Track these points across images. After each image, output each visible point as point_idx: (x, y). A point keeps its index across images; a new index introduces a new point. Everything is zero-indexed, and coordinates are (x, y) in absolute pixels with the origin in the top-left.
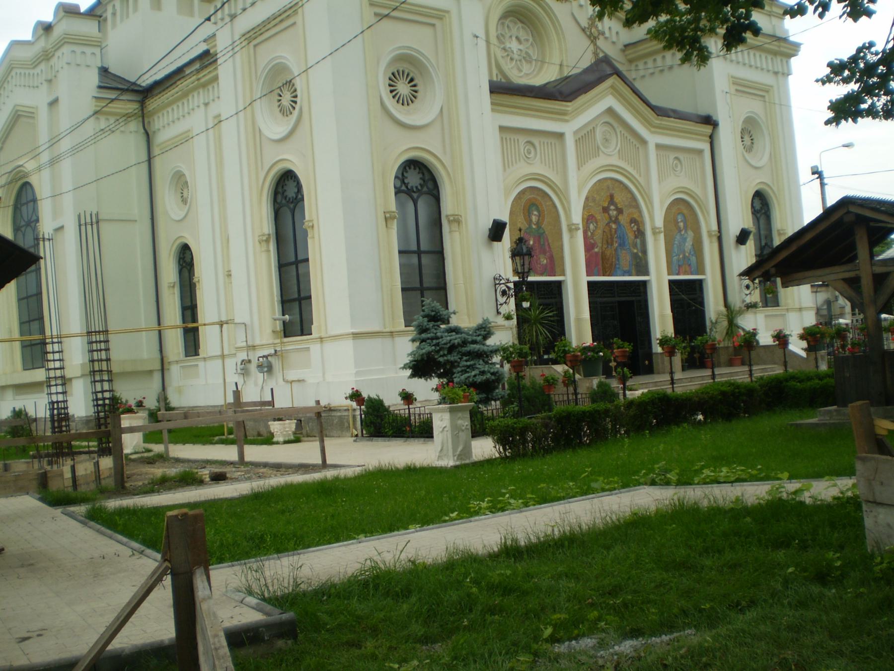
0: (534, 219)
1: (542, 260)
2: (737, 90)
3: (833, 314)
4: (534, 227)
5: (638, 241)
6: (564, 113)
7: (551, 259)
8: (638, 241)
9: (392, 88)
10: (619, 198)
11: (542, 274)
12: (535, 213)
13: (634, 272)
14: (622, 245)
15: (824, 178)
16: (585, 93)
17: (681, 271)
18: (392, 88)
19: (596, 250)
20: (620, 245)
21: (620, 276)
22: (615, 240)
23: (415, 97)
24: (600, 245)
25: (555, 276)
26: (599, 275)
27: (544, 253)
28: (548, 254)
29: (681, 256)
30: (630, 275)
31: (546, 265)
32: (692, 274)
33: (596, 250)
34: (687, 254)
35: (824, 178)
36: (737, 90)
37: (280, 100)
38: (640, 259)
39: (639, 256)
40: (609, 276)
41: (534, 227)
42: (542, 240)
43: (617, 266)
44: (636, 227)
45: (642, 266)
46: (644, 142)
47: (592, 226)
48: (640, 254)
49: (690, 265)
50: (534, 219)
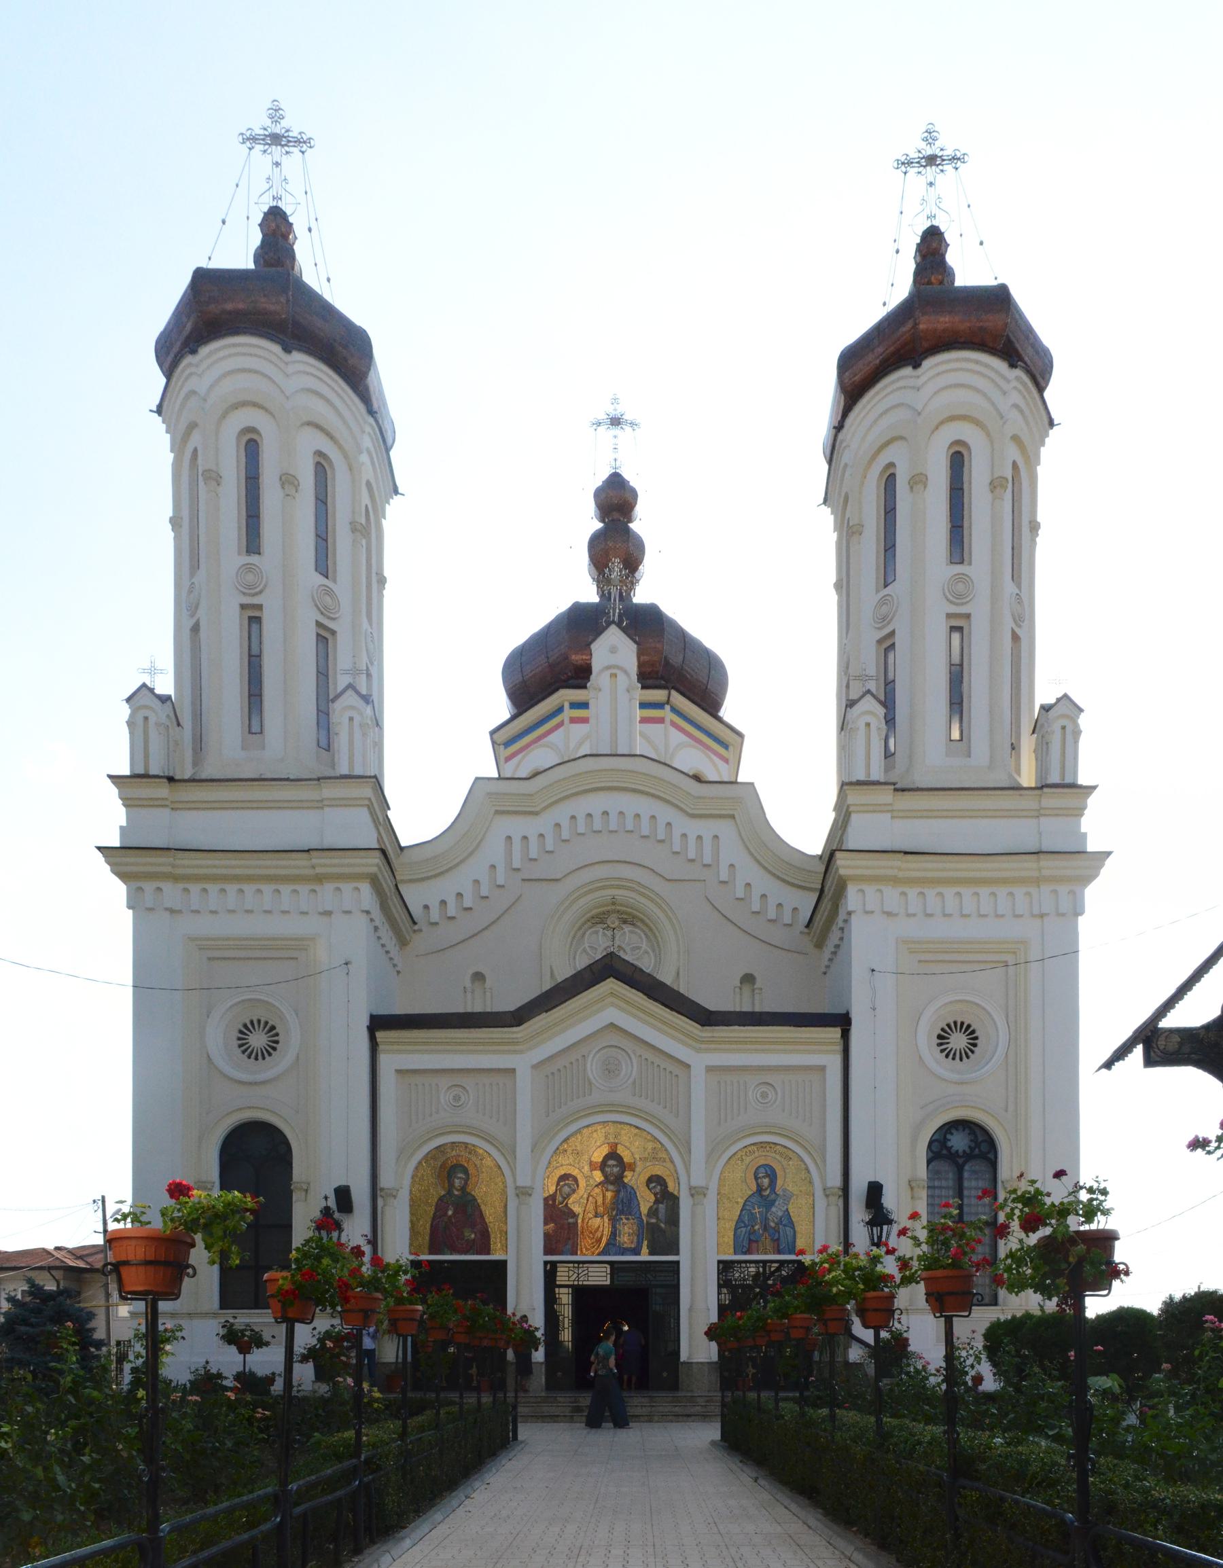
6: (515, 1042)
11: (466, 1253)
44: (659, 1187)
48: (663, 1225)
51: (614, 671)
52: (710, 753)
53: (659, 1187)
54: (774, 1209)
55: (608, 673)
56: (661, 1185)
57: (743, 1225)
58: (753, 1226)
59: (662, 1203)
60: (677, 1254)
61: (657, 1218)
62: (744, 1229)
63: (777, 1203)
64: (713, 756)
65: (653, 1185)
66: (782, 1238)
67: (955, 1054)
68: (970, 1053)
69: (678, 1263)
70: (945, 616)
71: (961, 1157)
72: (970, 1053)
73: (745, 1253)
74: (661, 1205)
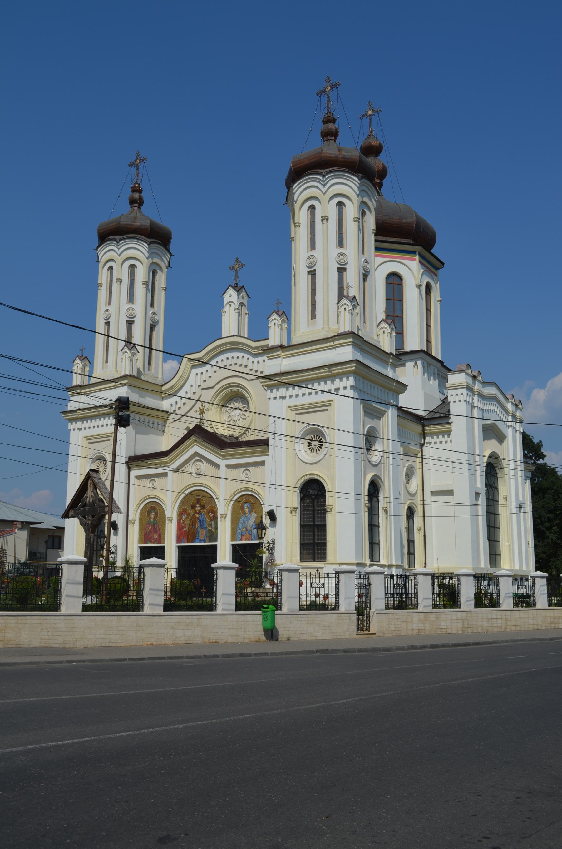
0: (152, 516)
1: (155, 536)
2: (297, 414)
3: (417, 634)
4: (152, 520)
5: (213, 522)
6: (167, 463)
7: (160, 536)
8: (213, 522)
9: (105, 470)
10: (204, 500)
11: (154, 543)
12: (153, 513)
13: (207, 540)
14: (202, 526)
15: (280, 371)
16: (488, 440)
17: (243, 538)
18: (105, 470)
19: (185, 529)
20: (200, 525)
21: (198, 543)
22: (197, 523)
23: (105, 471)
24: (187, 527)
25: (161, 543)
26: (185, 542)
27: (156, 532)
28: (158, 533)
29: (244, 529)
30: (205, 542)
31: (157, 538)
32: (252, 540)
33: (185, 529)
34: (249, 528)
35: (280, 371)
36: (297, 414)
37: (370, 445)
38: (213, 533)
39: (212, 531)
40: (191, 543)
41: (152, 520)
42: (155, 526)
43: (197, 537)
44: (212, 515)
45: (213, 536)
46: (218, 466)
47: (184, 517)
48: (213, 530)
49: (251, 535)
50: (152, 516)
51: (230, 303)
52: (432, 273)
53: (212, 515)
54: (250, 522)
55: (228, 305)
56: (213, 514)
57: (239, 529)
58: (242, 529)
59: (213, 521)
60: (216, 541)
61: (211, 527)
62: (239, 530)
63: (251, 519)
64: (432, 274)
65: (210, 513)
66: (252, 534)
67: (314, 450)
68: (320, 449)
69: (215, 546)
70: (126, 321)
71: (313, 495)
72: (320, 449)
73: (240, 541)
74: (213, 522)
